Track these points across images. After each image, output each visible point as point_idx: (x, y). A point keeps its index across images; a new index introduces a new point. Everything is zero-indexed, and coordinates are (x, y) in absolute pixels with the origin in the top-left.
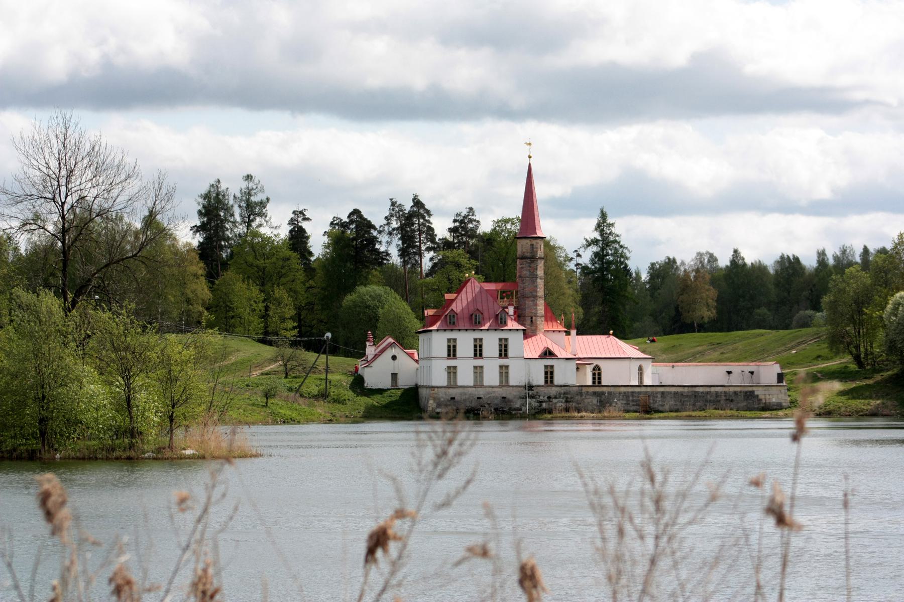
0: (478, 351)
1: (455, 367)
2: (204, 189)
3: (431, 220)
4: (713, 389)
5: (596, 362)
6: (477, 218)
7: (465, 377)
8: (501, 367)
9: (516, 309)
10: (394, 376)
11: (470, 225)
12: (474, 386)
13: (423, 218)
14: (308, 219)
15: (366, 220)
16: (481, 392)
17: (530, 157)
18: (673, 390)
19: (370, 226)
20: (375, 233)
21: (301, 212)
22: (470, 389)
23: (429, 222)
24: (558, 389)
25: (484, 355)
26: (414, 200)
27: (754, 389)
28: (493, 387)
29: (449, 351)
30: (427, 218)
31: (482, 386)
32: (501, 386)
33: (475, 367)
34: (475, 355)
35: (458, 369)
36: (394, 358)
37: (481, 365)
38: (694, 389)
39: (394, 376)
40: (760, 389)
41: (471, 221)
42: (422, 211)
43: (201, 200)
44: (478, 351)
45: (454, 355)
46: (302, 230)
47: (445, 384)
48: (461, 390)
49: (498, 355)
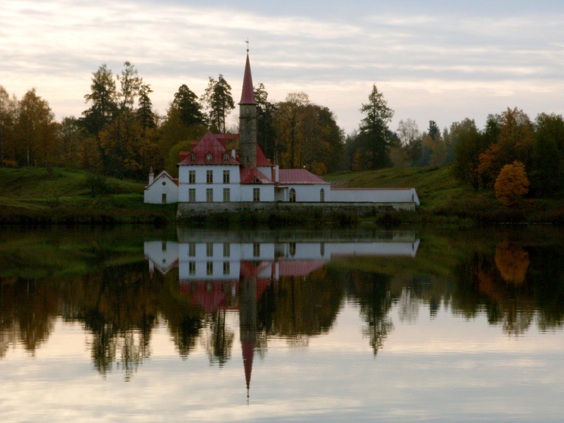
0: (210, 179)
1: (194, 190)
2: (96, 71)
3: (230, 91)
4: (365, 204)
5: (290, 187)
6: (265, 90)
7: (201, 196)
8: (208, 189)
9: (239, 152)
10: (164, 196)
11: (261, 96)
12: (207, 202)
13: (226, 90)
14: (149, 91)
15: (191, 92)
16: (211, 206)
17: (248, 51)
18: (338, 205)
19: (194, 96)
20: (197, 101)
21: (147, 87)
22: (204, 204)
23: (229, 93)
24: (262, 204)
25: (197, 181)
26: (220, 78)
27: (392, 205)
28: (219, 203)
29: (208, 179)
30: (228, 90)
31: (212, 202)
32: (224, 202)
33: (208, 189)
34: (208, 181)
35: (196, 190)
36: (164, 184)
37: (227, 188)
38: (352, 204)
39: (164, 196)
40: (396, 204)
41: (262, 92)
42: (224, 86)
43: (93, 77)
44: (210, 179)
45: (211, 181)
46: (147, 99)
47: (319, 201)
48: (197, 205)
49: (205, 181)
